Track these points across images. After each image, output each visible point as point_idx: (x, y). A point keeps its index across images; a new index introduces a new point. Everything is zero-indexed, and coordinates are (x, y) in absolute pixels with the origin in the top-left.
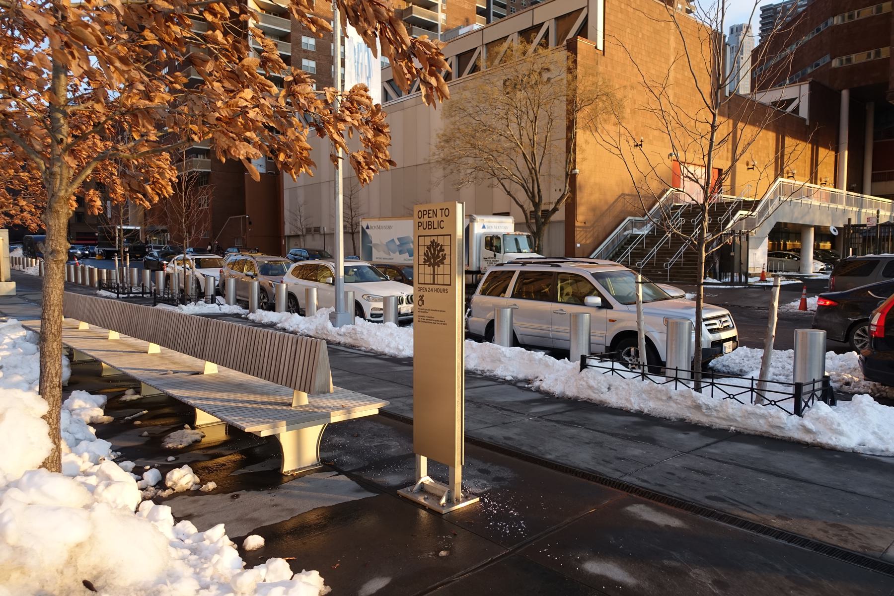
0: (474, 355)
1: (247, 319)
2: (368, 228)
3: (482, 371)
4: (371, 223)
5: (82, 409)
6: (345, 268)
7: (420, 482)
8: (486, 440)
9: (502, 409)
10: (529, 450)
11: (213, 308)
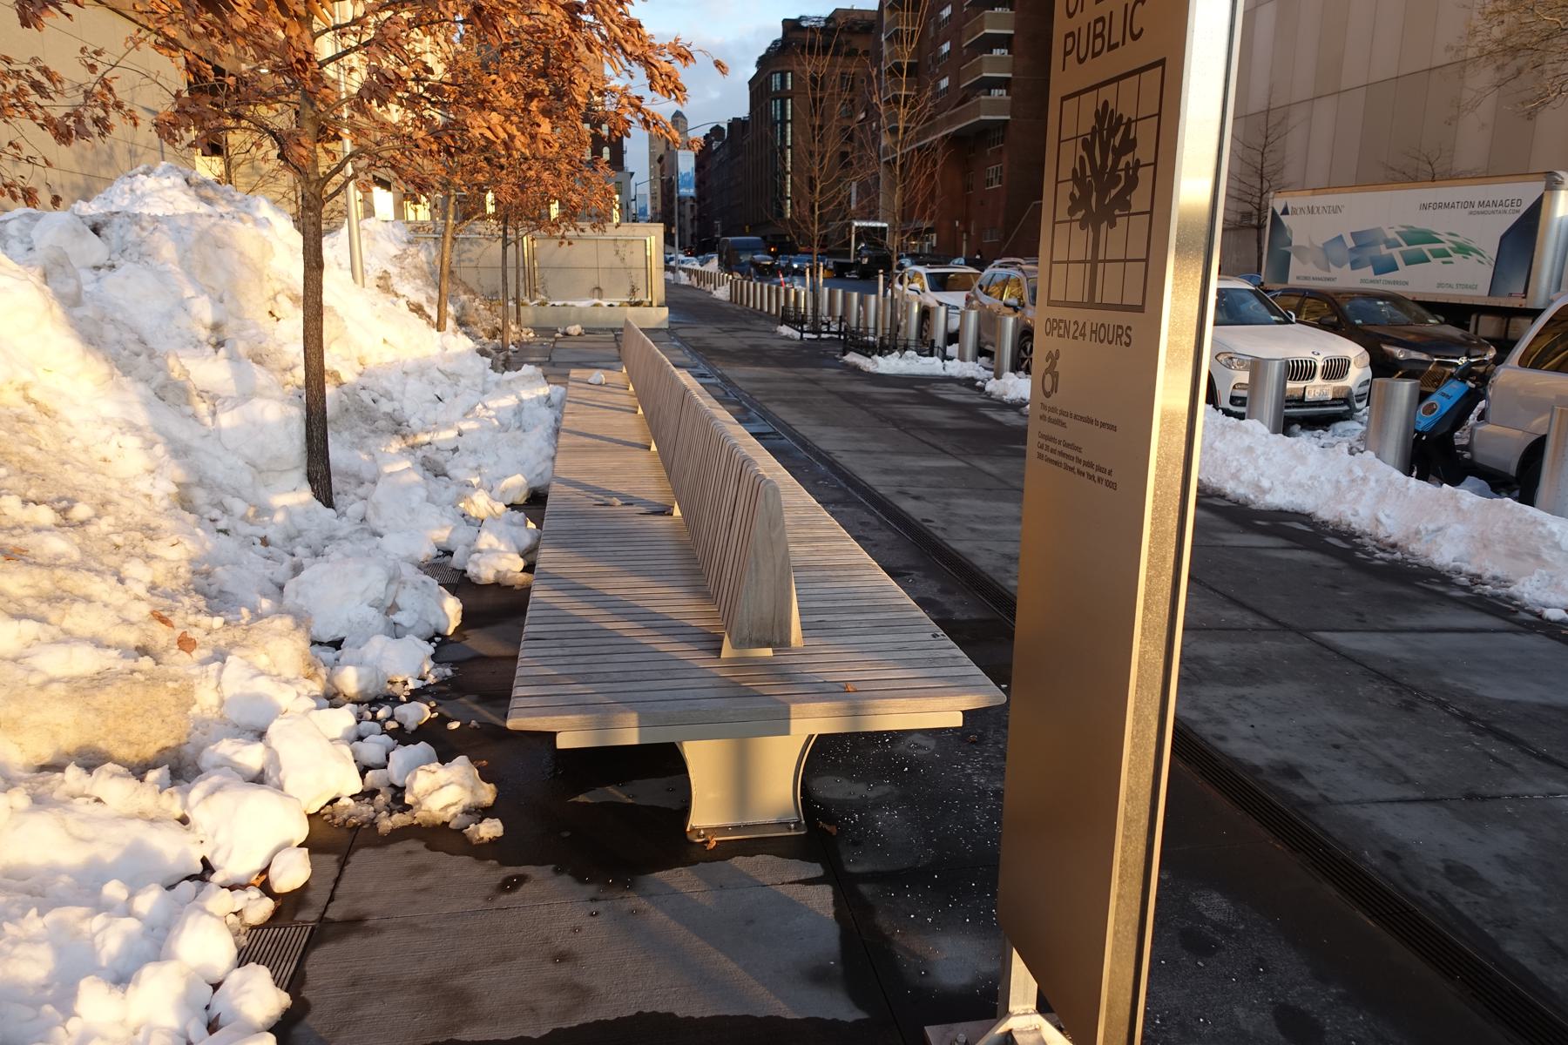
0: (1457, 529)
1: (982, 389)
2: (1285, 212)
3: (1476, 579)
4: (1295, 200)
5: (492, 551)
6: (1220, 292)
7: (1002, 1029)
8: (1372, 859)
9: (1489, 730)
10: (1531, 964)
11: (930, 366)
